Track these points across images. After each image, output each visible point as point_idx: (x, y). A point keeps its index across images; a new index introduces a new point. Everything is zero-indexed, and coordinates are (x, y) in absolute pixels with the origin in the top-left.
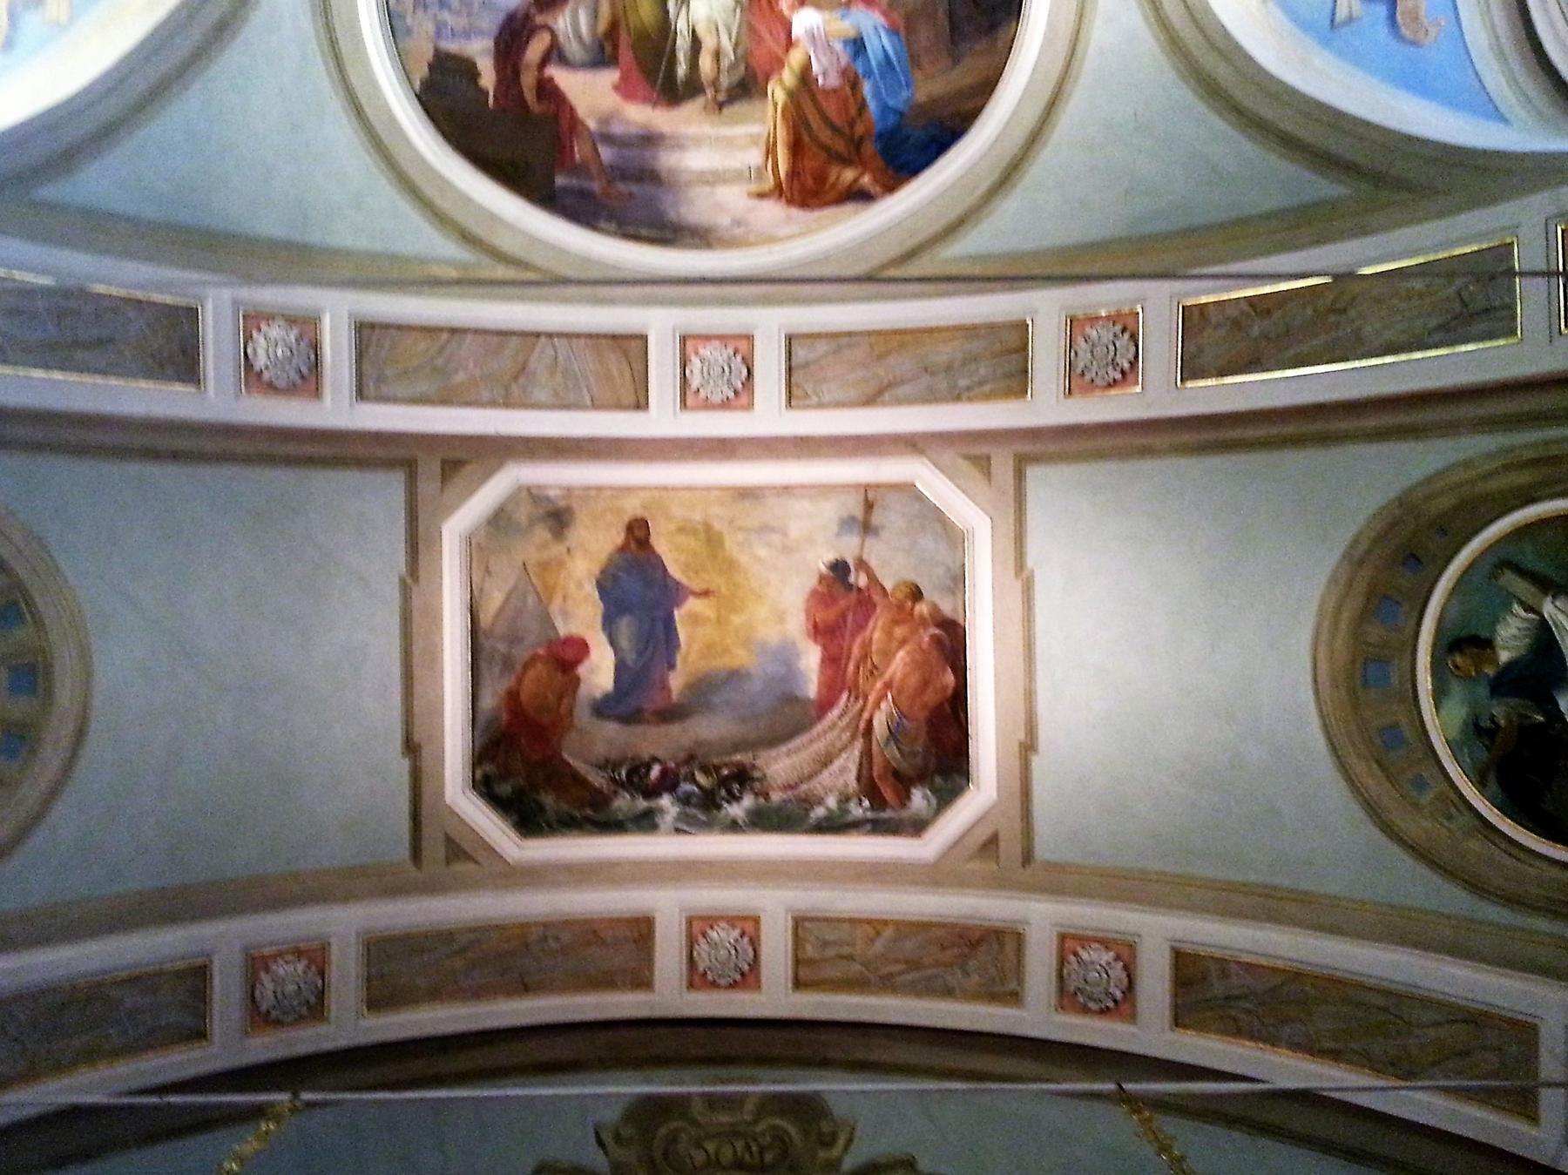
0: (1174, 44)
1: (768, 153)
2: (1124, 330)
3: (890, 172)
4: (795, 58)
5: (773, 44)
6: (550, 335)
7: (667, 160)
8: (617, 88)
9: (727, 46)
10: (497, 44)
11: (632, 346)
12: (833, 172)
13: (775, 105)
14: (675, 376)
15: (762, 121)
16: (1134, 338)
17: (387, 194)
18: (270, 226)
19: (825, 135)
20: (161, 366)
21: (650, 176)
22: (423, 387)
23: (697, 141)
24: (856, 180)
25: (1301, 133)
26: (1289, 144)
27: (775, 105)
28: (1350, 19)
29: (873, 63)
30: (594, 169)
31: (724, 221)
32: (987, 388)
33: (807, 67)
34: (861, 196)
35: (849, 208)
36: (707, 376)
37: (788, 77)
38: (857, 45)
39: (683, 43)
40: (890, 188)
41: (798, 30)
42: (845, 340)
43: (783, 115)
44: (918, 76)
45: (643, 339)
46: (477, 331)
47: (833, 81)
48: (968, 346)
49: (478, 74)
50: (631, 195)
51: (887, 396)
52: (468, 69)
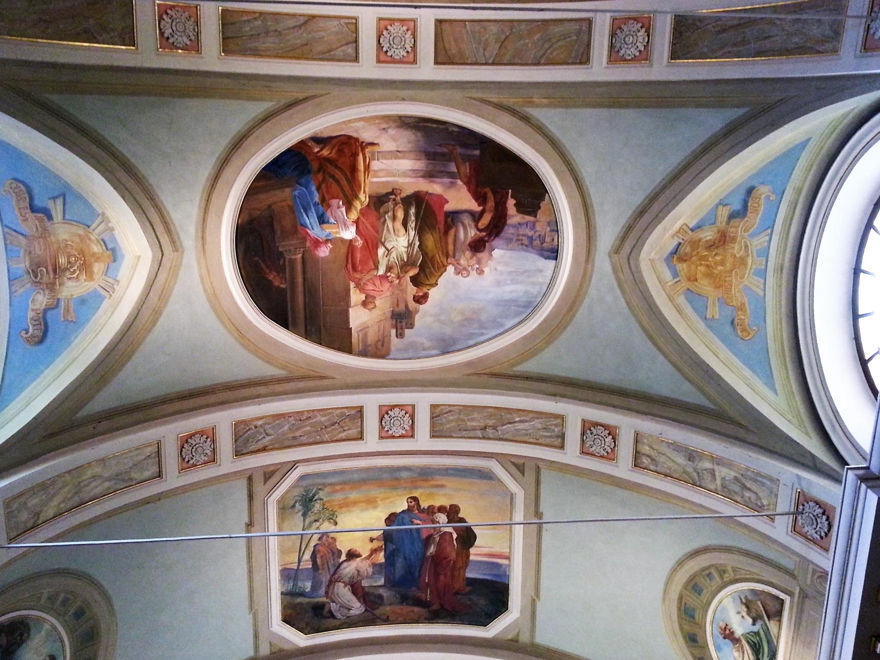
0: (152, 198)
1: (369, 167)
2: (168, 38)
3: (303, 152)
4: (354, 215)
5: (366, 223)
6: (486, 64)
7: (420, 165)
8: (447, 202)
9: (389, 223)
10: (506, 221)
11: (443, 58)
12: (333, 155)
13: (364, 192)
14: (420, 40)
15: (371, 182)
16: (162, 33)
17: (567, 141)
18: (630, 114)
19: (338, 174)
20: (693, 24)
21: (430, 156)
22: (557, 29)
23: (405, 174)
24: (322, 149)
25: (71, 131)
26: (82, 129)
27: (364, 192)
28: (54, 198)
29: (313, 209)
30: (460, 160)
31: (392, 132)
32: (245, 18)
33: (348, 210)
34: (317, 140)
35: (325, 135)
36: (402, 39)
37: (358, 205)
38: (322, 220)
39: (412, 224)
40: (302, 143)
41: (353, 229)
42: (325, 56)
43: (360, 187)
44: (290, 203)
45: (437, 63)
46: (527, 64)
47: (334, 202)
48: (256, 44)
49: (515, 205)
50: (440, 145)
51: (302, 19)
52: (521, 208)
